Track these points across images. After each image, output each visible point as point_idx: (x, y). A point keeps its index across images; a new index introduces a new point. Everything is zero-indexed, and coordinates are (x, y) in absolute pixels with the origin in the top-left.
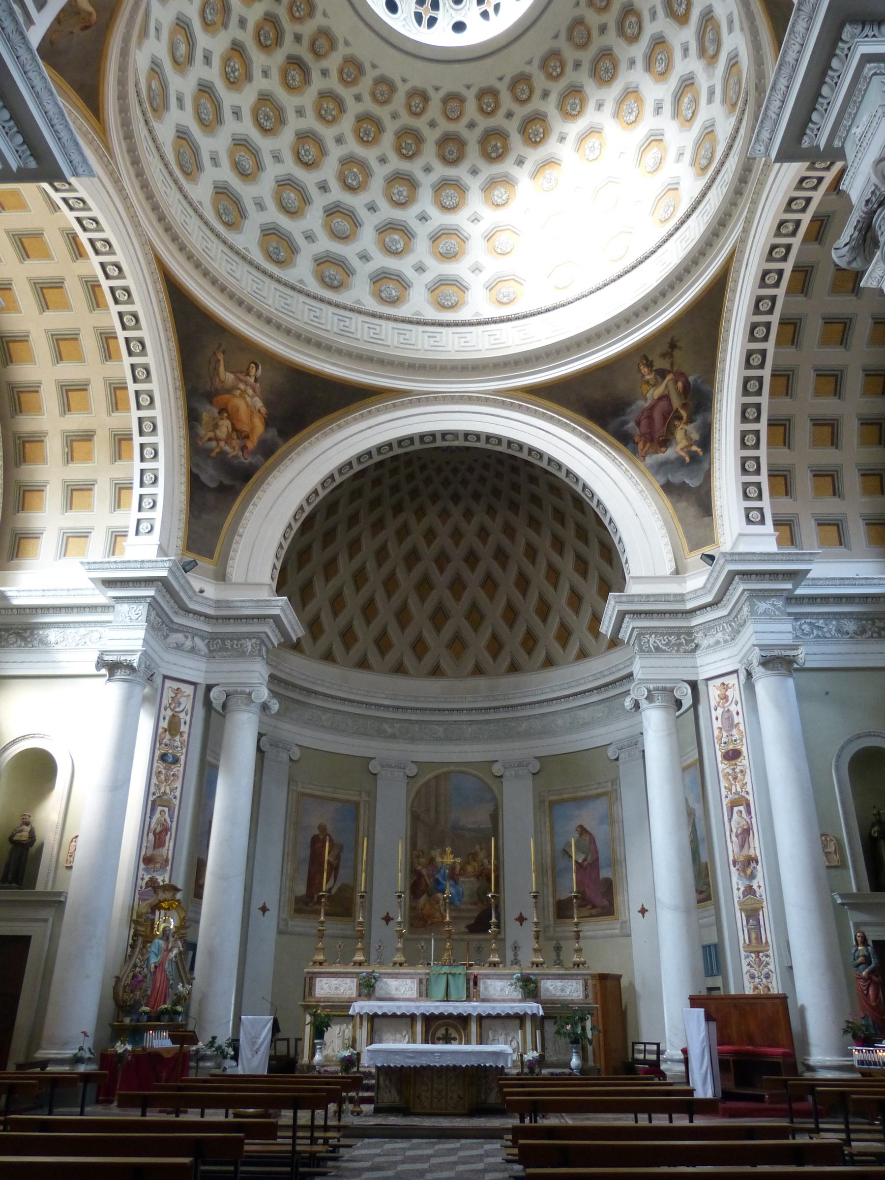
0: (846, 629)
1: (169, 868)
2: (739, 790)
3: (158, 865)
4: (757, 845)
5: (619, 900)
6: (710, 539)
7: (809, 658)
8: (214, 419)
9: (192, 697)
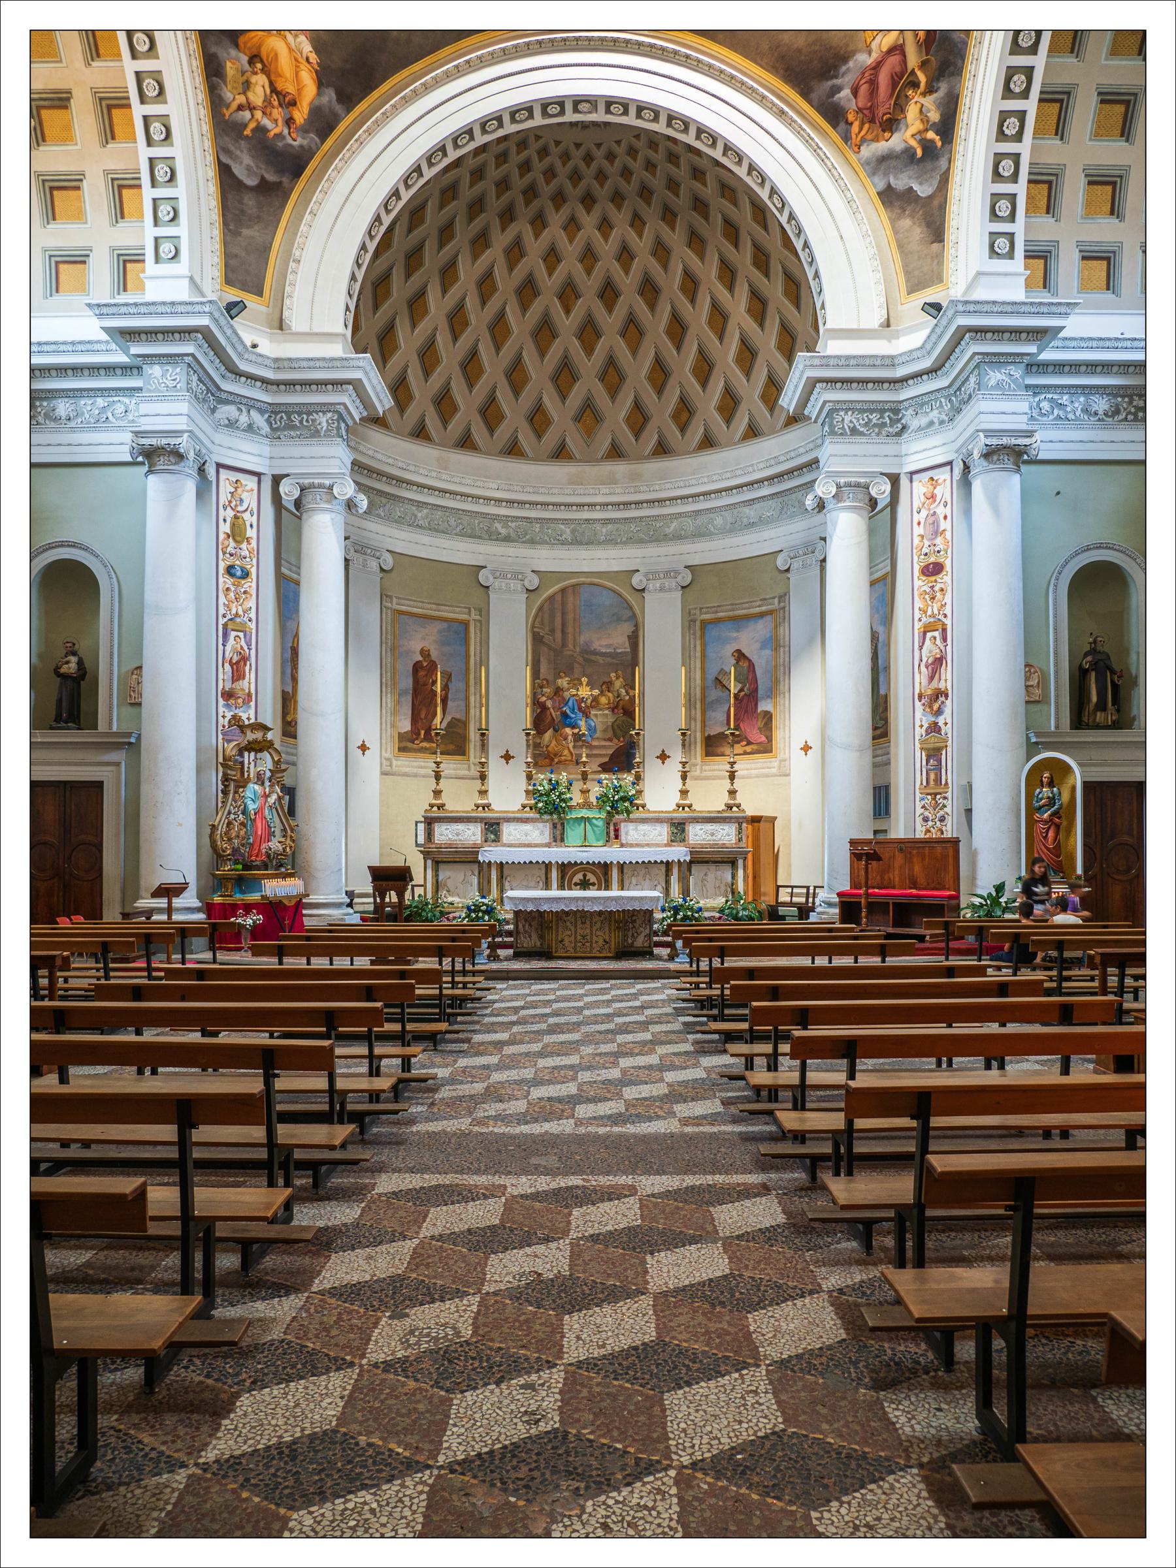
0: (1095, 407)
1: (253, 704)
2: (936, 612)
3: (240, 701)
4: (949, 677)
5: (778, 735)
6: (936, 277)
7: (1044, 446)
8: (243, 73)
9: (256, 492)
